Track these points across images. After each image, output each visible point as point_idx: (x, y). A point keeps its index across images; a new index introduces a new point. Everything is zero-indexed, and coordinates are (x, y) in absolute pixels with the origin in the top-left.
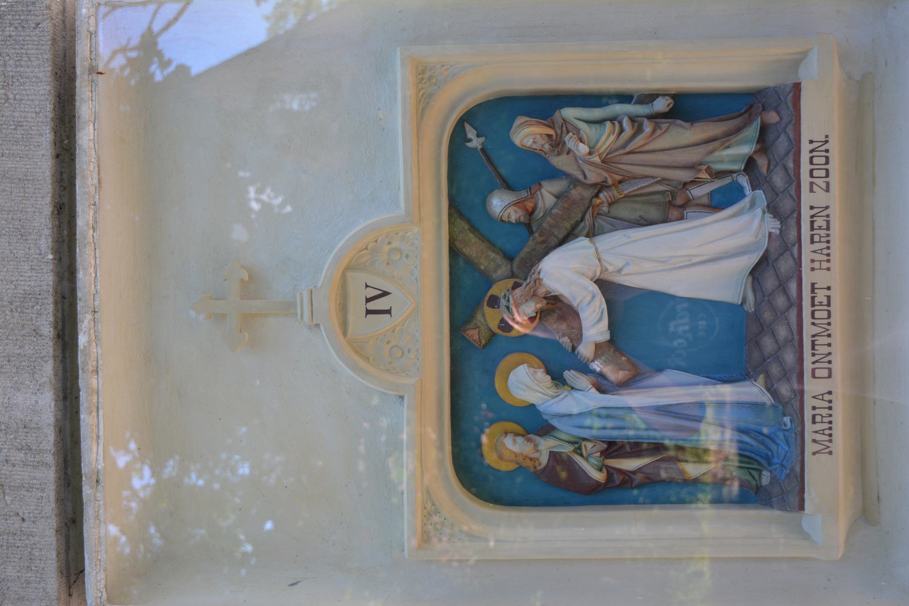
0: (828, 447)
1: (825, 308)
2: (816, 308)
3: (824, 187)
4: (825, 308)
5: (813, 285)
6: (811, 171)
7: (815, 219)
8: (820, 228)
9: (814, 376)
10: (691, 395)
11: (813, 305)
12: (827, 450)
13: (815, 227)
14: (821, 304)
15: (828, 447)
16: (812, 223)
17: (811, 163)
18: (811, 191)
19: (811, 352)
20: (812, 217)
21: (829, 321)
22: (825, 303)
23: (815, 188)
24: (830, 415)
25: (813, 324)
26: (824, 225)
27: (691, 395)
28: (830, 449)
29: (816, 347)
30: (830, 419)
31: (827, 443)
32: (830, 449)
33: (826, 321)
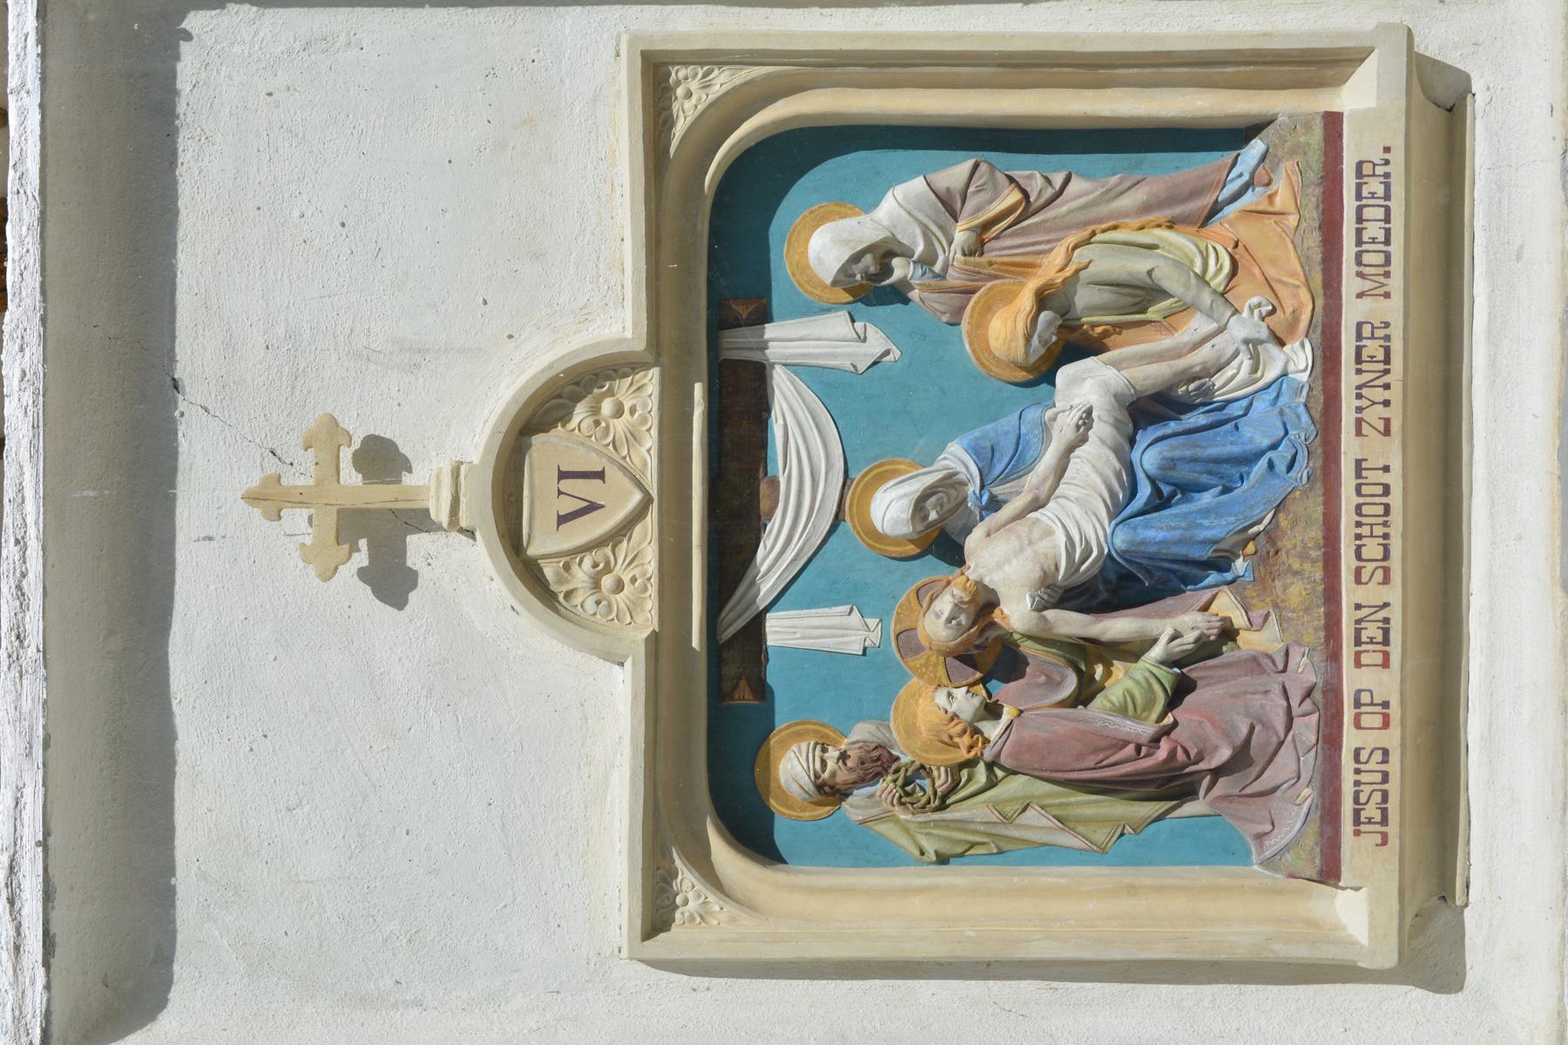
0: (1383, 285)
1: (1382, 247)
2: (1365, 247)
3: (1381, 427)
4: (1382, 202)
5: (1358, 463)
6: (1359, 507)
7: (1363, 625)
8: (1374, 241)
9: (1358, 664)
10: (1160, 357)
11: (1359, 242)
12: (1381, 291)
13: (1365, 239)
14: (1370, 821)
15: (1383, 285)
16: (1358, 632)
17: (1359, 493)
18: (1359, 432)
19: (1353, 366)
20: (1358, 622)
21: (1384, 829)
22: (1378, 819)
23: (1366, 429)
24: (1387, 162)
25: (1360, 275)
26: (1379, 637)
27: (1160, 357)
28: (1385, 289)
29: (1364, 473)
30: (1386, 331)
31: (1382, 279)
32: (1385, 289)
33: (1381, 270)
